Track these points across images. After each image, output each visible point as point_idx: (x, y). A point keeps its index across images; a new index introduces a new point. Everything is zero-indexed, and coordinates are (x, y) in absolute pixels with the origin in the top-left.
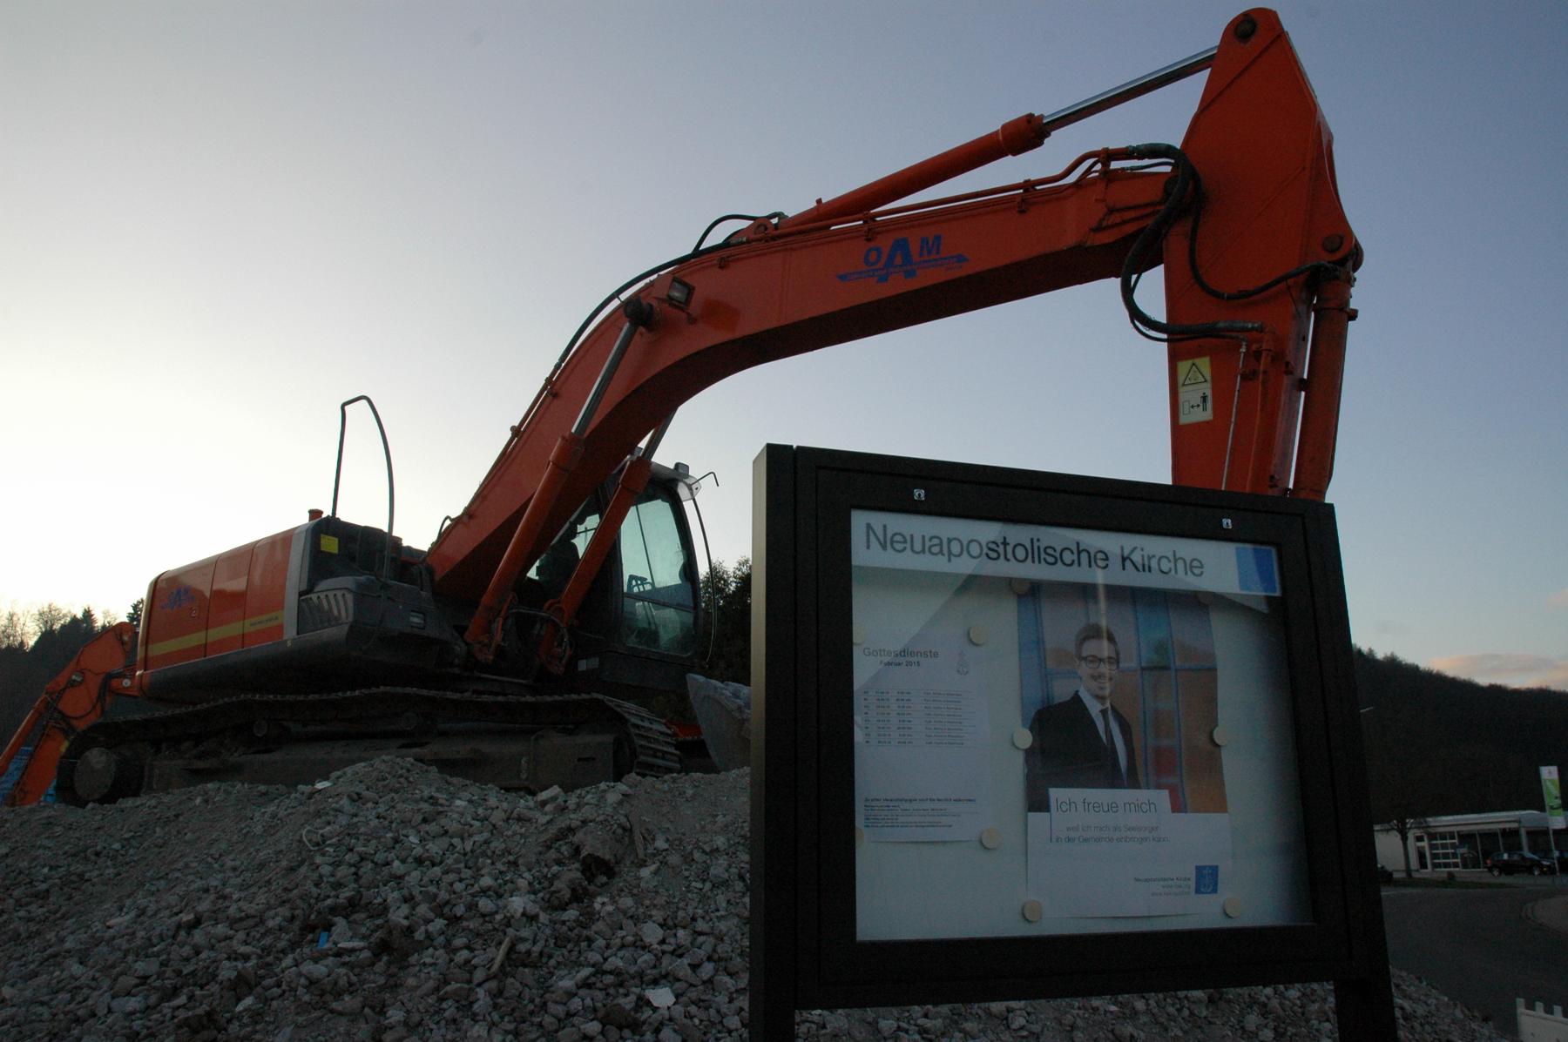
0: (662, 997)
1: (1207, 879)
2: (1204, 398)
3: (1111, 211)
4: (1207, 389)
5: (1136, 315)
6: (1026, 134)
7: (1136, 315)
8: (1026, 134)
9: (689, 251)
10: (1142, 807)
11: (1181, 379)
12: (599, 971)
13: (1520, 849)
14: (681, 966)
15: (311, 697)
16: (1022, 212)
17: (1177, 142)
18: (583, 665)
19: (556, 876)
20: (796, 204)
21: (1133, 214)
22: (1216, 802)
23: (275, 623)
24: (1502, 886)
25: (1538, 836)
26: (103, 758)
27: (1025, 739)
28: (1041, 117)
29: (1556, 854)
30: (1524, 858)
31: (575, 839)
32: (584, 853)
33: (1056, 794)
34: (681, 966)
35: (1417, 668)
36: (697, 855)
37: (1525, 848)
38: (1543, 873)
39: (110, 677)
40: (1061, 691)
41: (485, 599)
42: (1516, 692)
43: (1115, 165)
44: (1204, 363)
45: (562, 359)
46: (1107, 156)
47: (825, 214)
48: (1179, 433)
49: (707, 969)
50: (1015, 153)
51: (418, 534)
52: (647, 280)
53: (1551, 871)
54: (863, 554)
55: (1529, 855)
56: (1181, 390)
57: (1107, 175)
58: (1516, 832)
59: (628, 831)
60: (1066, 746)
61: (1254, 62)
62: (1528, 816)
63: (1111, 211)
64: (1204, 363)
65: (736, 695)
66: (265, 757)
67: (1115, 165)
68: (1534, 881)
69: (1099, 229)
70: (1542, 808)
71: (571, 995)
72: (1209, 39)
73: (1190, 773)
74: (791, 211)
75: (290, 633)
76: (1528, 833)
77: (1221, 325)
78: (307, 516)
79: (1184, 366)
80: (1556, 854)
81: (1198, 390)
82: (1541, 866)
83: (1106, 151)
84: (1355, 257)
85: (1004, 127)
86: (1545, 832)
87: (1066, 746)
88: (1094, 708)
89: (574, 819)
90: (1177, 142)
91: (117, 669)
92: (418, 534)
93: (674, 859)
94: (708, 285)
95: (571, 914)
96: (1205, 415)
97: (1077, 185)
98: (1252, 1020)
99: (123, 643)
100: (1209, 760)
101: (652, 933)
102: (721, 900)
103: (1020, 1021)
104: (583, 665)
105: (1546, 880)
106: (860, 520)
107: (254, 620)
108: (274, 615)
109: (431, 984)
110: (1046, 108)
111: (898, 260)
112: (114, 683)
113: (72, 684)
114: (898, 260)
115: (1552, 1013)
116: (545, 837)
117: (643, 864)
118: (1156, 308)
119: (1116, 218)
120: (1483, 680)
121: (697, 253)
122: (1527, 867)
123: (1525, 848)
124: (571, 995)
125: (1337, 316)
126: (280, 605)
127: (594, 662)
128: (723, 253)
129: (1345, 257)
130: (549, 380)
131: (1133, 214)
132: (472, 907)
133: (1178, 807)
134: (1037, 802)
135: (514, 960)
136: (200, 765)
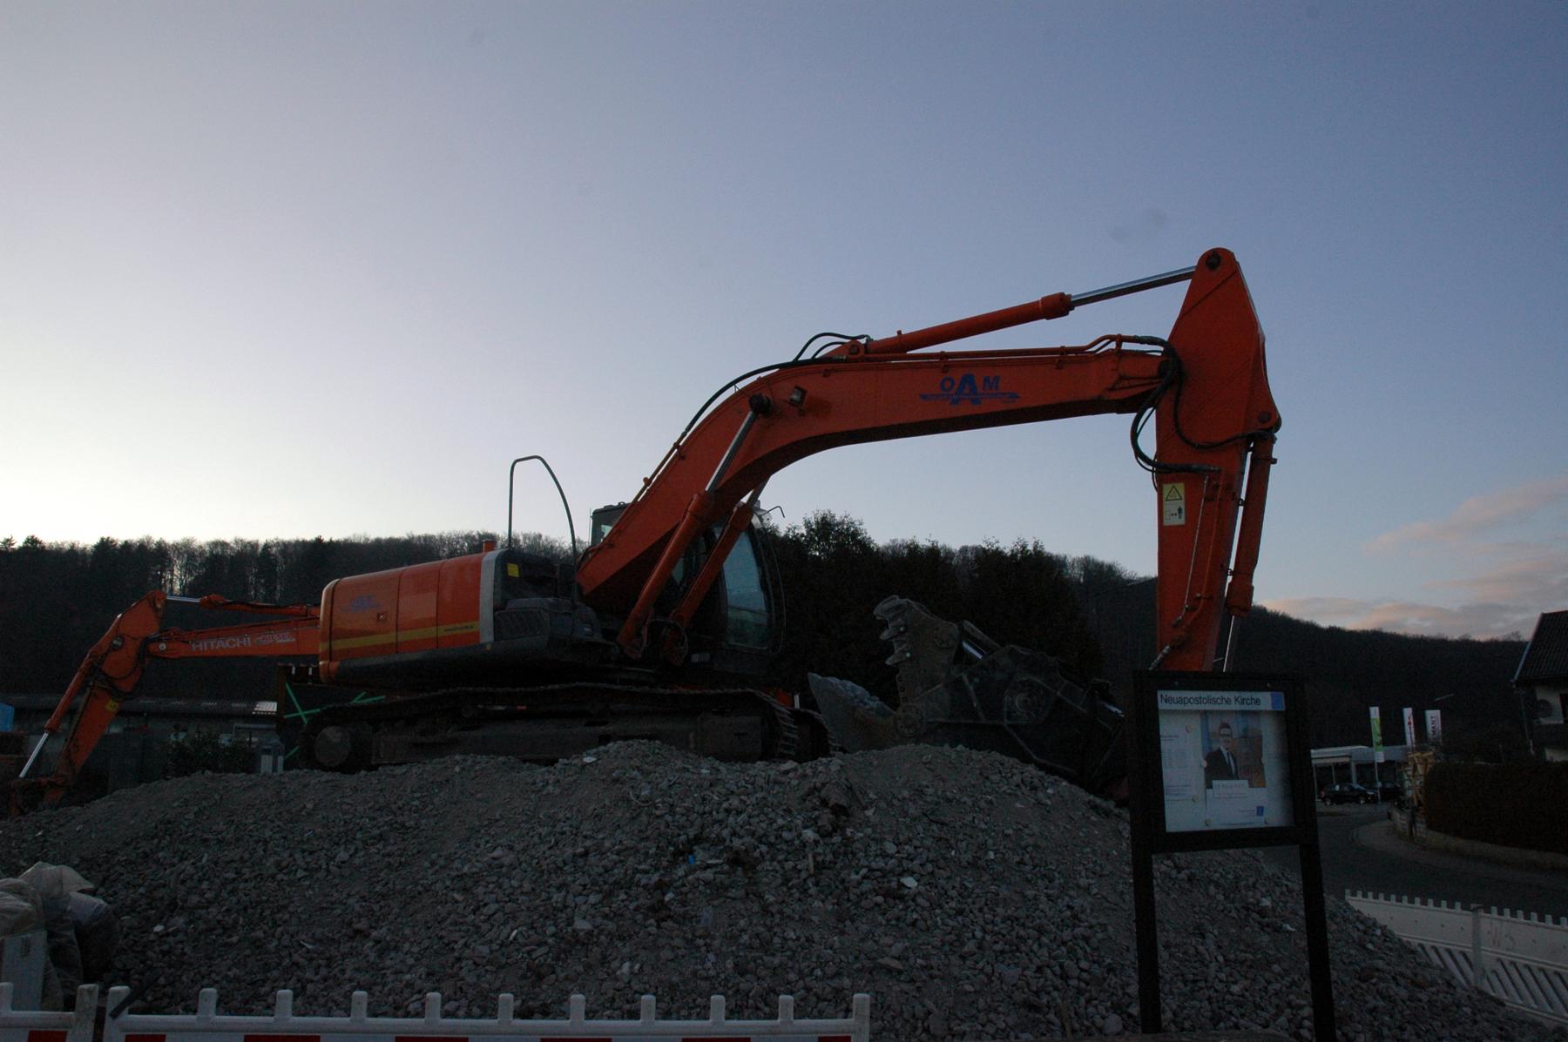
0: (910, 882)
1: (1260, 811)
3: (1121, 378)
4: (1182, 504)
5: (1139, 454)
6: (1058, 306)
7: (1139, 454)
8: (1058, 306)
9: (790, 359)
10: (1240, 786)
12: (871, 870)
13: (1349, 779)
14: (915, 865)
18: (695, 658)
19: (818, 817)
20: (881, 331)
22: (1262, 784)
24: (1333, 814)
25: (1366, 768)
27: (1205, 764)
28: (1070, 296)
29: (1379, 784)
30: (1352, 789)
31: (823, 793)
32: (831, 803)
33: (1215, 783)
34: (915, 865)
35: (1265, 610)
36: (895, 802)
37: (1354, 778)
38: (1367, 802)
39: (147, 641)
40: (1215, 747)
41: (633, 611)
42: (1352, 634)
43: (1126, 346)
44: (1181, 487)
45: (688, 429)
46: (1120, 339)
48: (1165, 533)
49: (929, 867)
50: (1049, 317)
52: (763, 375)
53: (1374, 800)
54: (1162, 706)
55: (1357, 786)
57: (1119, 352)
58: (1346, 766)
59: (850, 788)
60: (1217, 768)
61: (1216, 281)
62: (1358, 749)
64: (1181, 487)
65: (853, 690)
66: (473, 733)
68: (1364, 809)
69: (1112, 389)
70: (1371, 745)
71: (860, 883)
72: (1191, 261)
73: (1253, 773)
74: (877, 336)
75: (487, 637)
76: (1358, 766)
79: (1167, 488)
80: (1379, 784)
81: (1176, 504)
82: (1366, 796)
84: (1277, 424)
85: (1044, 299)
86: (1371, 765)
87: (1217, 768)
88: (1225, 752)
89: (818, 781)
91: (153, 634)
93: (883, 805)
94: (815, 386)
95: (837, 839)
96: (1179, 521)
98: (1212, 889)
99: (157, 610)
100: (1260, 769)
101: (891, 848)
102: (920, 828)
103: (1095, 891)
104: (695, 658)
105: (1369, 808)
106: (1159, 693)
108: (469, 624)
109: (779, 881)
110: (1074, 291)
112: (152, 647)
113: (114, 648)
115: (1489, 912)
116: (799, 794)
117: (865, 808)
118: (1149, 445)
119: (1126, 383)
120: (1324, 623)
121: (796, 363)
122: (1354, 797)
123: (1354, 778)
124: (860, 883)
125: (1264, 461)
126: (472, 612)
127: (707, 656)
128: (829, 366)
129: (1271, 421)
130: (676, 445)
132: (779, 837)
133: (1251, 786)
134: (1209, 786)
135: (820, 867)
136: (423, 739)
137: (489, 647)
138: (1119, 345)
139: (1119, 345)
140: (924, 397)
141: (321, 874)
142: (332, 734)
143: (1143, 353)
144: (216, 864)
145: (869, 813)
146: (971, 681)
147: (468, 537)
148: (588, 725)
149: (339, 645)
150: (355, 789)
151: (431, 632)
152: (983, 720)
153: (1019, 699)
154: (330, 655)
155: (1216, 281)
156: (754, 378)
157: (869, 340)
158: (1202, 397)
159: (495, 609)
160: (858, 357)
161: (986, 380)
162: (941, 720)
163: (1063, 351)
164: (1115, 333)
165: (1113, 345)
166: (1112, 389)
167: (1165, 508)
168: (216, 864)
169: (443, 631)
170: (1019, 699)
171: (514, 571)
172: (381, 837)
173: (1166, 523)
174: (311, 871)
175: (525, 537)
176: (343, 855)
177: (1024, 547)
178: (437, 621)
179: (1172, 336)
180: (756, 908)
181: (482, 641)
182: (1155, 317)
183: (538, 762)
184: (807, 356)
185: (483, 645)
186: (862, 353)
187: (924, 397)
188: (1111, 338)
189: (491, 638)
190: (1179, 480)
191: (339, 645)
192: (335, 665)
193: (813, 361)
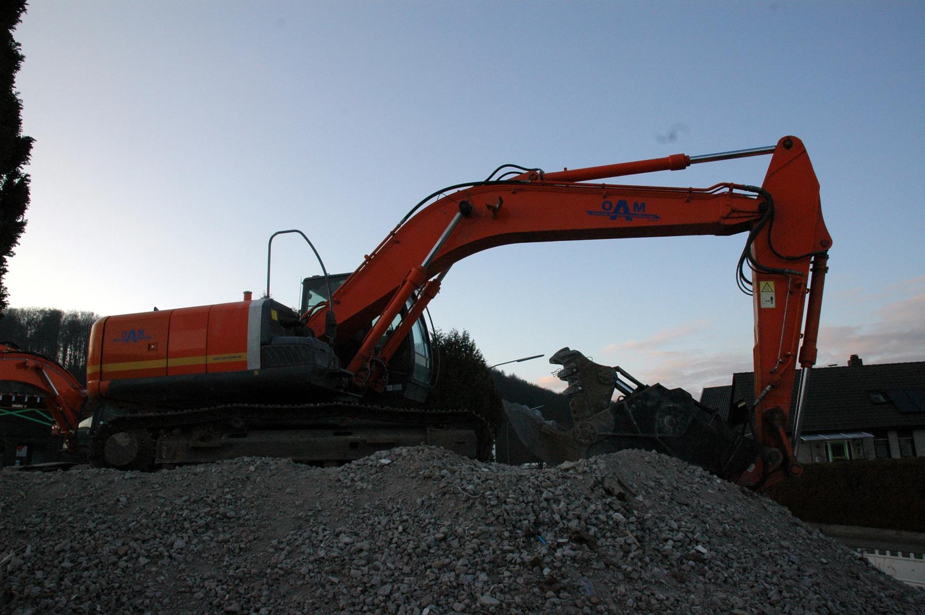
2: (772, 299)
3: (733, 211)
6: (679, 163)
8: (679, 163)
9: (483, 179)
11: (761, 289)
15: (285, 406)
16: (688, 201)
17: (760, 185)
20: (551, 166)
21: (747, 215)
23: (242, 359)
26: (128, 439)
43: (735, 191)
44: (771, 284)
45: (402, 222)
46: (732, 186)
47: (568, 179)
51: (864, 363)
56: (762, 294)
57: (730, 193)
61: (790, 156)
63: (733, 211)
64: (771, 284)
67: (735, 191)
72: (774, 142)
74: (547, 171)
77: (787, 270)
78: (243, 295)
79: (762, 284)
83: (732, 184)
85: (671, 157)
90: (760, 185)
92: (864, 363)
97: (716, 195)
107: (215, 356)
110: (691, 153)
111: (622, 210)
114: (622, 210)
115: (909, 556)
117: (635, 495)
121: (487, 183)
125: (820, 271)
126: (244, 348)
127: (399, 387)
130: (392, 233)
131: (747, 215)
136: (203, 444)
137: (256, 373)
138: (731, 190)
139: (731, 190)
140: (590, 213)
141: (166, 561)
142: (121, 439)
143: (745, 196)
144: (43, 553)
145: (640, 498)
146: (629, 407)
147: (42, 311)
148: (335, 434)
149: (110, 367)
150: (162, 485)
151: (200, 360)
152: (640, 434)
153: (666, 419)
154: (100, 375)
155: (790, 156)
156: (455, 191)
157: (542, 172)
158: (782, 229)
159: (262, 344)
160: (533, 182)
161: (636, 205)
162: (609, 433)
163: (690, 190)
164: (730, 182)
165: (727, 190)
166: (726, 218)
167: (762, 297)
168: (43, 553)
169: (211, 359)
170: (666, 419)
171: (275, 315)
172: (207, 526)
173: (763, 306)
174: (154, 559)
175: (83, 314)
176: (180, 543)
177: (456, 334)
178: (206, 351)
179: (765, 184)
180: (621, 577)
181: (249, 368)
182: (753, 174)
183: (312, 463)
184: (494, 179)
185: (252, 371)
186: (539, 181)
187: (590, 213)
188: (726, 185)
189: (258, 366)
190: (771, 279)
191: (110, 367)
192: (105, 384)
193: (498, 182)
